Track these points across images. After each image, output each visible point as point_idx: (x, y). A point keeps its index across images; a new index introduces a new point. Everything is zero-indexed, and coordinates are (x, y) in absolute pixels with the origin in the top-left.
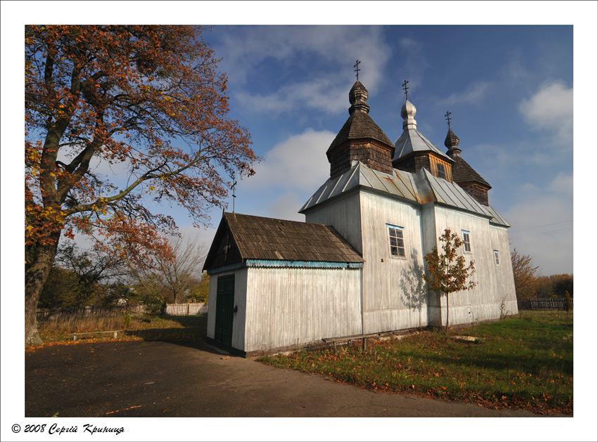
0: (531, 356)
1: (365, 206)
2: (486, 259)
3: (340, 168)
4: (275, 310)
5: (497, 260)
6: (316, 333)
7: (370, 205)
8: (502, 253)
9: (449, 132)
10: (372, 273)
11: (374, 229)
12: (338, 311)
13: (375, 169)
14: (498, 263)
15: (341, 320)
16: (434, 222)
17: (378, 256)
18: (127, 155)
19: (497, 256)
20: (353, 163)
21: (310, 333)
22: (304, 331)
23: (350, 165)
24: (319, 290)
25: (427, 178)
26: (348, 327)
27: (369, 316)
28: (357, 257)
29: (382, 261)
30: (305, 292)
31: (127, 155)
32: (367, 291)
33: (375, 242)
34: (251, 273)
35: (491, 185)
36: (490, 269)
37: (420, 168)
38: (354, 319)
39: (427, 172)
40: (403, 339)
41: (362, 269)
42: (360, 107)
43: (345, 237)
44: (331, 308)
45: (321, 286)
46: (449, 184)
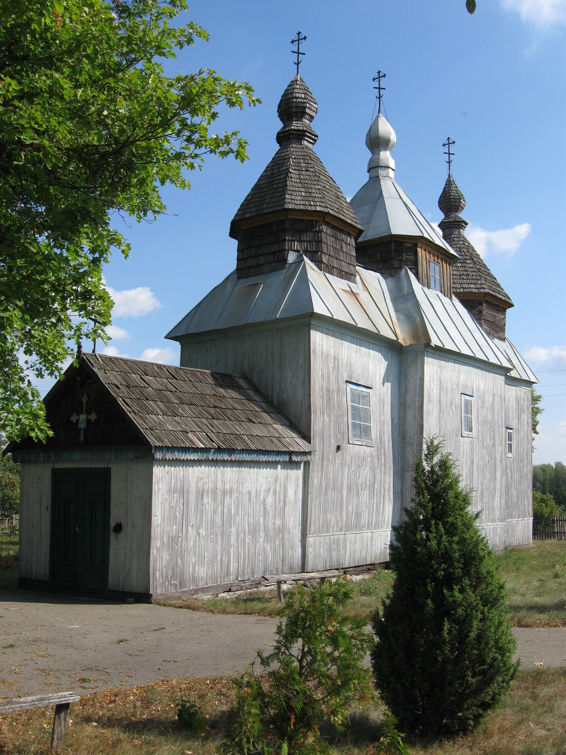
0: (37, 49)
1: (318, 348)
2: (494, 445)
3: (262, 260)
4: (188, 530)
5: (510, 445)
6: (241, 569)
7: (325, 346)
8: (518, 432)
9: (449, 183)
10: (322, 471)
11: (328, 391)
12: (271, 533)
13: (329, 273)
14: (510, 450)
15: (275, 548)
16: (422, 379)
17: (333, 441)
18: (99, 336)
19: (510, 439)
20: (292, 257)
21: (233, 568)
22: (225, 568)
23: (285, 260)
24: (246, 498)
25: (413, 292)
26: (283, 560)
27: (315, 543)
28: (301, 444)
29: (338, 448)
30: (227, 500)
31: (99, 336)
32: (313, 502)
33: (329, 416)
34: (158, 471)
35: (513, 301)
36: (498, 464)
37: (400, 268)
38: (292, 547)
39: (412, 276)
40: (428, 591)
41: (307, 464)
42: (300, 135)
43: (255, 379)
44: (262, 528)
45: (250, 493)
46: (446, 300)
